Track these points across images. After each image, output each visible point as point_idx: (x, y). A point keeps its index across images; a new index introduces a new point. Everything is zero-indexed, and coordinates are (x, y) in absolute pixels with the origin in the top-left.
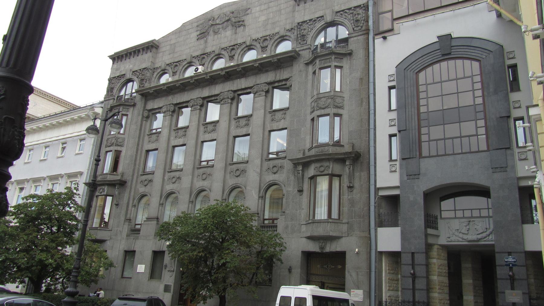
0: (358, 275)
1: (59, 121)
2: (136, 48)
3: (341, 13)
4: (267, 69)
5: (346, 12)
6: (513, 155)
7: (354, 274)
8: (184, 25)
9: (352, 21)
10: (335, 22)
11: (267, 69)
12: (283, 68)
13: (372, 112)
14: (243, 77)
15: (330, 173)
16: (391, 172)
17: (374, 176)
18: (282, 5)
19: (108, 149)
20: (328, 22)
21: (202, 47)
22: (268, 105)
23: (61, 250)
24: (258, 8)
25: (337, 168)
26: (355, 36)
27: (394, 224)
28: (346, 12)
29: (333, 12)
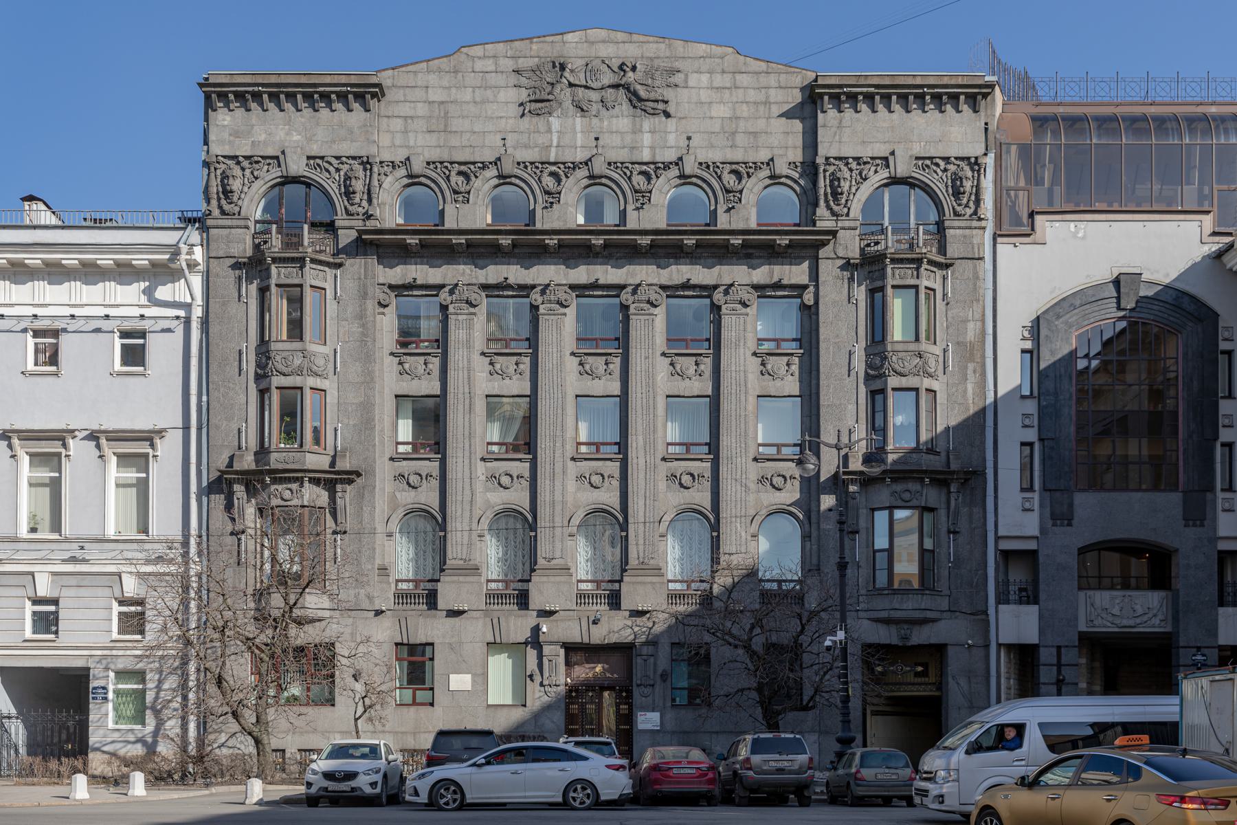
0: (970, 682)
3: (928, 162)
6: (1214, 501)
7: (963, 682)
12: (790, 257)
15: (923, 504)
18: (772, 92)
24: (705, 78)
25: (932, 496)
26: (959, 228)
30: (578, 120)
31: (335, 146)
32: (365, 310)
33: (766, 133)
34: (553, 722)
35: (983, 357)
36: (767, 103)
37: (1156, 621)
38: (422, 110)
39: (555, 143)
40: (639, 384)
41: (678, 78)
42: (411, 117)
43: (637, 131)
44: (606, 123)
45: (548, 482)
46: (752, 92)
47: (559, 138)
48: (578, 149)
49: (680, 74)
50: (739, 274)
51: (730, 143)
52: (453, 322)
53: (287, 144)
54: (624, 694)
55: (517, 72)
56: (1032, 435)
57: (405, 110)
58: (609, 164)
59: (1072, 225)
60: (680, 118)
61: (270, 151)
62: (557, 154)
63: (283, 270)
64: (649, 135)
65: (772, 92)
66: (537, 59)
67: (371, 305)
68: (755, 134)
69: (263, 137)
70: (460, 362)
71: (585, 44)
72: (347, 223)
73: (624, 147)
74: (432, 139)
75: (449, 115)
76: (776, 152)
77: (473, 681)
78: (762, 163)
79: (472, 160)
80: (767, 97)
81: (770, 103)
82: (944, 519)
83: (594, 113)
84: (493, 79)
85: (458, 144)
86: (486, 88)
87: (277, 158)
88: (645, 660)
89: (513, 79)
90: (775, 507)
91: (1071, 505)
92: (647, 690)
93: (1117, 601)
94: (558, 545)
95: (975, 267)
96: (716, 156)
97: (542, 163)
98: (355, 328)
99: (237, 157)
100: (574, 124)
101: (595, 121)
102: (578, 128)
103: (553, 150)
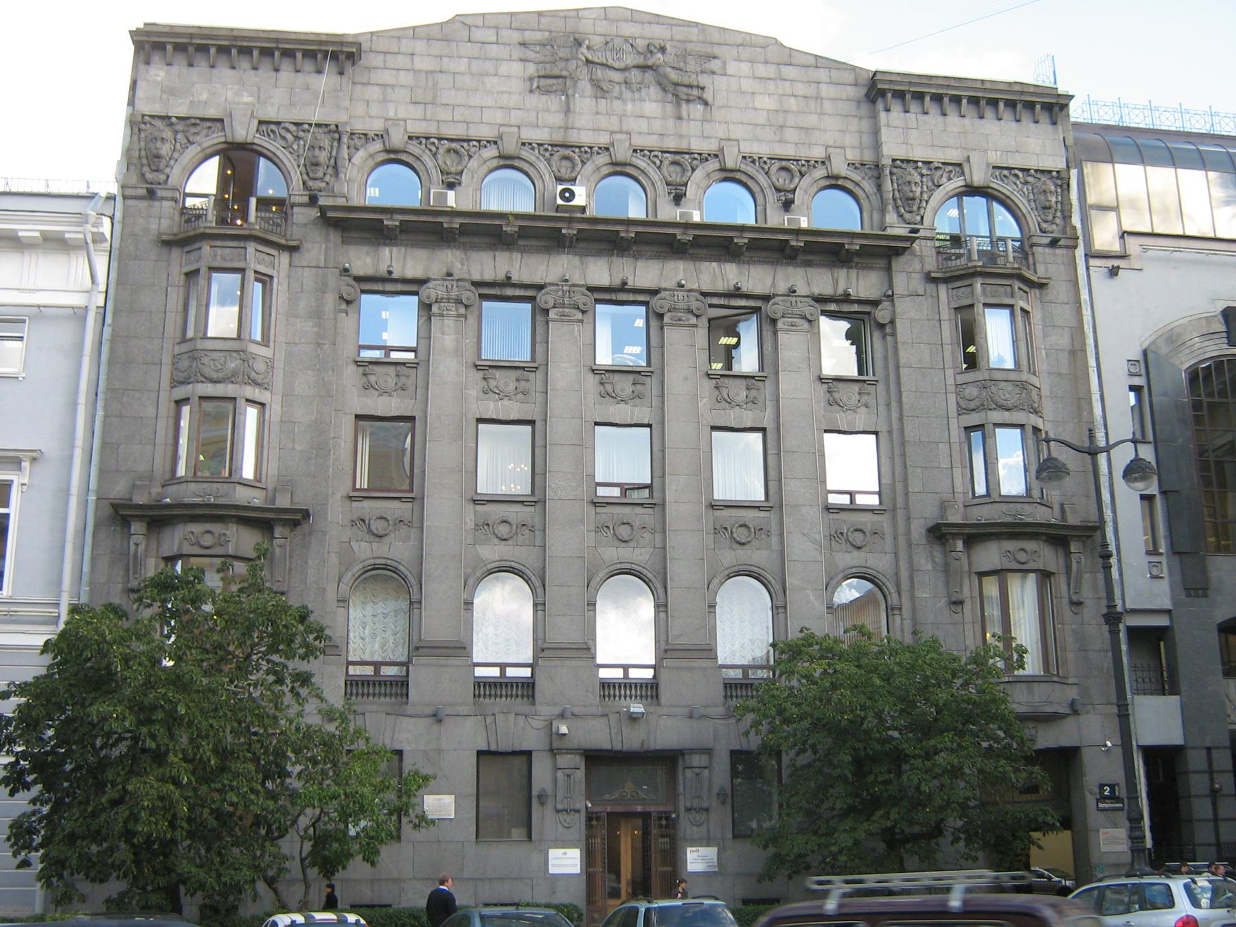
1: (65, 232)
2: (342, 44)
3: (1006, 172)
5: (1016, 176)
8: (464, 23)
9: (1033, 204)
16: (1154, 577)
19: (181, 392)
20: (976, 184)
21: (557, 119)
22: (469, 341)
24: (745, 67)
28: (1016, 176)
29: (988, 165)
36: (818, 98)
41: (715, 65)
42: (393, 86)
49: (716, 61)
51: (777, 138)
55: (523, 44)
57: (386, 77)
58: (635, 151)
61: (212, 113)
63: (219, 251)
65: (823, 88)
67: (330, 300)
74: (417, 112)
80: (818, 92)
81: (822, 99)
82: (1064, 587)
87: (221, 121)
89: (518, 52)
90: (854, 570)
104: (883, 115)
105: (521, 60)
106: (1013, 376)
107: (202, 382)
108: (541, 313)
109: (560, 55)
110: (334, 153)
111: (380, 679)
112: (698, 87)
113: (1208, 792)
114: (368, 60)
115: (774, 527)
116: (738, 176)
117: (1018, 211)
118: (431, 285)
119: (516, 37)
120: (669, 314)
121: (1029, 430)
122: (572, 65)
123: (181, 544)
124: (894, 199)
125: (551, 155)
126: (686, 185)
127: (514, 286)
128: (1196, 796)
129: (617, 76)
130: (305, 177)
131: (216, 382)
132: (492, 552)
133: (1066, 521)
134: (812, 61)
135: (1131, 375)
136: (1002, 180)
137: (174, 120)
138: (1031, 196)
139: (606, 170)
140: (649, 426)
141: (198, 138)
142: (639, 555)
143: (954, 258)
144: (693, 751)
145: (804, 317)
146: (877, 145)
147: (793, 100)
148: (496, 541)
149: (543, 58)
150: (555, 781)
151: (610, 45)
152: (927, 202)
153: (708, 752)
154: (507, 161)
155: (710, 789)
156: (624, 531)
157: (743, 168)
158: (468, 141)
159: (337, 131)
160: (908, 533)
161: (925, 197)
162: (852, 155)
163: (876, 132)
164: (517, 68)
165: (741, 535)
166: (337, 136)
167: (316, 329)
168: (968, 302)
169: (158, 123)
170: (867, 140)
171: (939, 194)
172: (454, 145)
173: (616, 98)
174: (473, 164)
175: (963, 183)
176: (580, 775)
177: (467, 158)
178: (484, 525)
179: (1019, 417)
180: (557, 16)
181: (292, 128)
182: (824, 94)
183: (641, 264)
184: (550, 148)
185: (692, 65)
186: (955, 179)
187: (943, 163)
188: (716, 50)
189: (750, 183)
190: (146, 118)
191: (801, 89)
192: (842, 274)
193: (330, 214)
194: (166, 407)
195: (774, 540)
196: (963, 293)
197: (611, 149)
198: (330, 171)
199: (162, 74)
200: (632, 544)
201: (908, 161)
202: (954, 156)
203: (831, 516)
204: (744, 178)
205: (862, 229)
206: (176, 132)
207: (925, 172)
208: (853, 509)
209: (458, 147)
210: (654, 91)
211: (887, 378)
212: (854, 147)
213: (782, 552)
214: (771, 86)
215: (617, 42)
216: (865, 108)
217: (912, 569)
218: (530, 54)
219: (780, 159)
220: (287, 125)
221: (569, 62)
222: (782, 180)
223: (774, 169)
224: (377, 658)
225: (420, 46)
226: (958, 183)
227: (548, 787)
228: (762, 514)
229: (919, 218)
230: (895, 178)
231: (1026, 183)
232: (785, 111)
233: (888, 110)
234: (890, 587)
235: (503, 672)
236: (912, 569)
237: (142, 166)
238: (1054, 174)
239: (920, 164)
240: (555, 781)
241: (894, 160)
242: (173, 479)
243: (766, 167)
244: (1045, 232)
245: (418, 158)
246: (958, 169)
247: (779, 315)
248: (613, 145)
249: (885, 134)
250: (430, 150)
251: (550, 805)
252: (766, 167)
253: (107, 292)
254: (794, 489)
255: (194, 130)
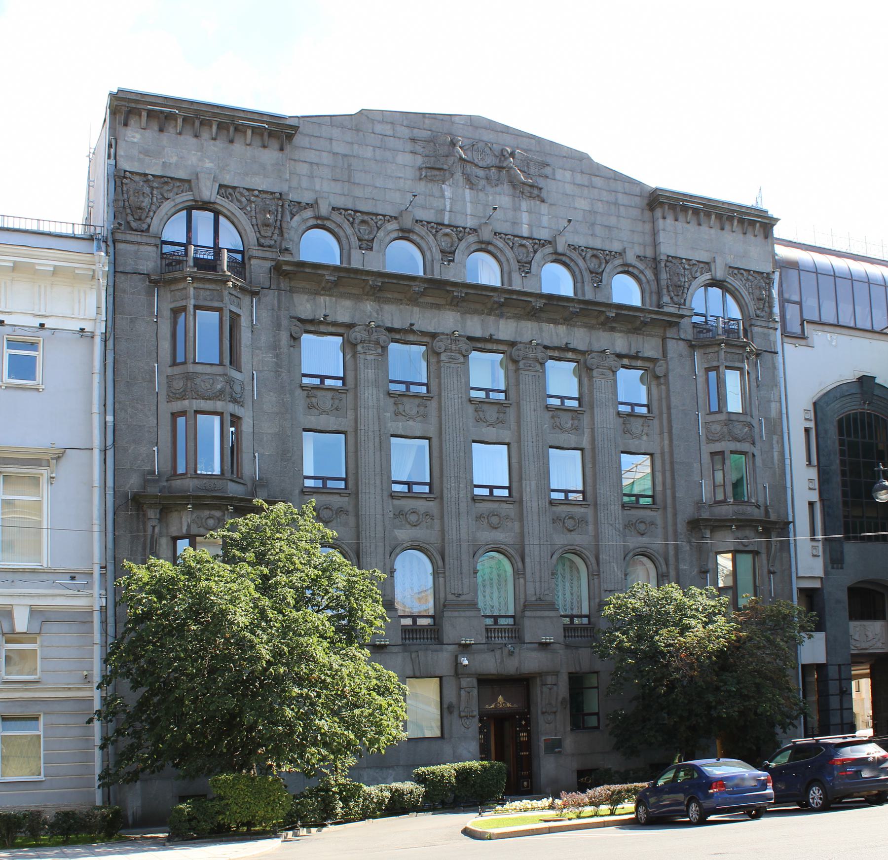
3: (736, 271)
4: (614, 325)
5: (742, 274)
8: (364, 115)
10: (725, 284)
11: (614, 325)
12: (643, 334)
13: (788, 462)
14: (561, 324)
16: (814, 556)
17: (108, 547)
19: (177, 406)
23: (631, 645)
24: (568, 174)
25: (754, 541)
26: (761, 326)
27: (819, 628)
28: (742, 274)
30: (467, 191)
31: (248, 179)
32: (279, 341)
33: (617, 228)
34: (469, 752)
35: (782, 431)
36: (616, 204)
37: (879, 645)
38: (326, 158)
39: (448, 208)
40: (530, 433)
41: (548, 171)
42: (317, 164)
43: (516, 209)
44: (490, 198)
45: (454, 521)
46: (605, 193)
47: (451, 204)
48: (469, 217)
49: (548, 167)
50: (620, 342)
51: (590, 232)
52: (362, 361)
53: (199, 170)
54: (523, 723)
55: (413, 140)
56: (815, 496)
57: (312, 156)
58: (495, 234)
59: (829, 335)
60: (551, 205)
61: (181, 174)
62: (450, 218)
63: (202, 292)
64: (527, 213)
65: (620, 196)
66: (429, 132)
67: (284, 337)
68: (609, 227)
69: (174, 160)
70: (370, 401)
71: (470, 128)
72: (260, 254)
73: (507, 221)
74: (337, 188)
75: (352, 168)
76: (626, 244)
77: (446, 709)
78: (616, 253)
79: (375, 211)
80: (616, 199)
81: (619, 205)
82: (765, 562)
83: (480, 187)
84: (391, 143)
85: (361, 195)
86: (385, 149)
87: (189, 181)
88: (550, 689)
89: (409, 146)
90: (639, 550)
91: (842, 553)
92: (550, 718)
93: (858, 629)
94: (466, 581)
95: (773, 358)
96: (581, 241)
97: (438, 224)
98: (269, 358)
99: (146, 175)
100: (464, 194)
101: (481, 195)
102: (468, 198)
103: (447, 214)
104: (661, 221)
105: (412, 152)
106: (742, 418)
107: (196, 399)
108: (433, 354)
109: (441, 152)
110: (279, 218)
111: (418, 627)
112: (537, 187)
113: (838, 692)
114: (298, 140)
115: (590, 519)
116: (564, 258)
117: (743, 301)
118: (357, 329)
119: (405, 132)
120: (524, 361)
121: (750, 455)
122: (451, 160)
123: (189, 526)
124: (668, 287)
125: (437, 232)
126: (530, 263)
127: (328, 324)
128: (832, 695)
129: (481, 173)
130: (258, 235)
131: (207, 399)
132: (403, 534)
133: (769, 518)
134: (612, 175)
135: (806, 419)
136: (734, 277)
137: (150, 177)
138: (751, 291)
139: (474, 247)
140: (344, 433)
141: (170, 195)
142: (502, 537)
143: (705, 331)
144: (547, 673)
145: (610, 369)
146: (655, 244)
147: (599, 204)
148: (408, 526)
149: (427, 153)
150: (459, 696)
151: (475, 147)
152: (155, 212)
153: (556, 673)
154: (405, 234)
155: (557, 699)
156: (495, 520)
157: (568, 253)
158: (377, 215)
159: (281, 198)
160: (675, 524)
161: (154, 208)
162: (638, 250)
163: (655, 233)
164: (407, 158)
165: (570, 523)
166: (280, 203)
167: (275, 360)
168: (715, 364)
169: (137, 178)
170: (648, 239)
171: (167, 206)
172: (366, 218)
173: (481, 190)
174: (381, 234)
175: (709, 277)
176: (475, 692)
177: (376, 228)
178: (400, 514)
179: (219, 405)
180: (435, 119)
181: (246, 193)
182: (620, 202)
183: (502, 322)
184: (435, 226)
185: (533, 170)
186: (706, 274)
187: (698, 261)
188: (549, 160)
189: (499, 254)
190: (127, 173)
191: (605, 196)
192: (634, 338)
193: (285, 268)
194: (165, 420)
195: (591, 528)
196: (712, 357)
197: (479, 231)
198: (277, 231)
199: (138, 136)
200: (499, 530)
201: (676, 258)
202: (704, 257)
203: (625, 512)
204: (568, 261)
205: (341, 263)
206: (152, 188)
207: (687, 267)
208: (566, 502)
209: (369, 219)
210: (506, 188)
211: (661, 414)
212: (640, 244)
213: (358, 526)
214: (586, 191)
215: (481, 145)
216: (647, 214)
217: (677, 548)
218: (418, 148)
219: (592, 249)
220: (241, 190)
221: (449, 159)
222: (593, 264)
223: (589, 255)
224: (496, 613)
225: (336, 132)
226: (707, 277)
227: (454, 700)
228: (582, 510)
229: (683, 301)
230: (668, 269)
231: (748, 280)
232: (594, 212)
233: (664, 218)
234: (591, 559)
235: (415, 622)
236: (677, 548)
237: (127, 215)
238: (613, 253)
239: (684, 261)
240: (459, 696)
241: (668, 256)
242: (174, 475)
243: (584, 254)
244: (758, 317)
245: (422, 238)
246: (707, 266)
247: (594, 367)
248: (625, 252)
249: (662, 237)
250: (348, 220)
251: (456, 714)
252: (584, 254)
253: (106, 321)
254: (530, 487)
255: (166, 188)
